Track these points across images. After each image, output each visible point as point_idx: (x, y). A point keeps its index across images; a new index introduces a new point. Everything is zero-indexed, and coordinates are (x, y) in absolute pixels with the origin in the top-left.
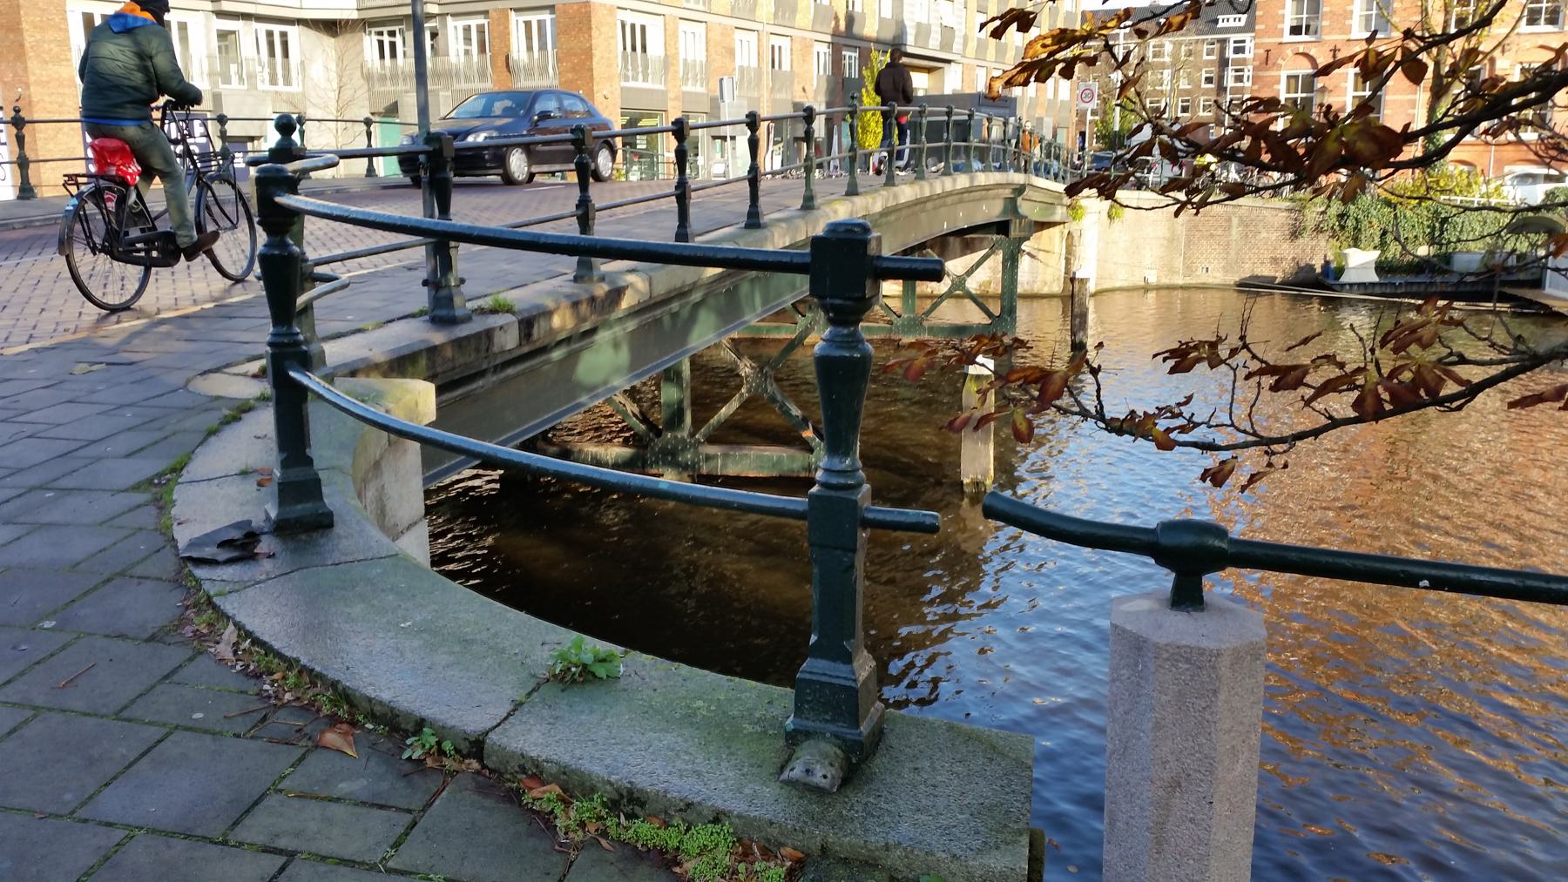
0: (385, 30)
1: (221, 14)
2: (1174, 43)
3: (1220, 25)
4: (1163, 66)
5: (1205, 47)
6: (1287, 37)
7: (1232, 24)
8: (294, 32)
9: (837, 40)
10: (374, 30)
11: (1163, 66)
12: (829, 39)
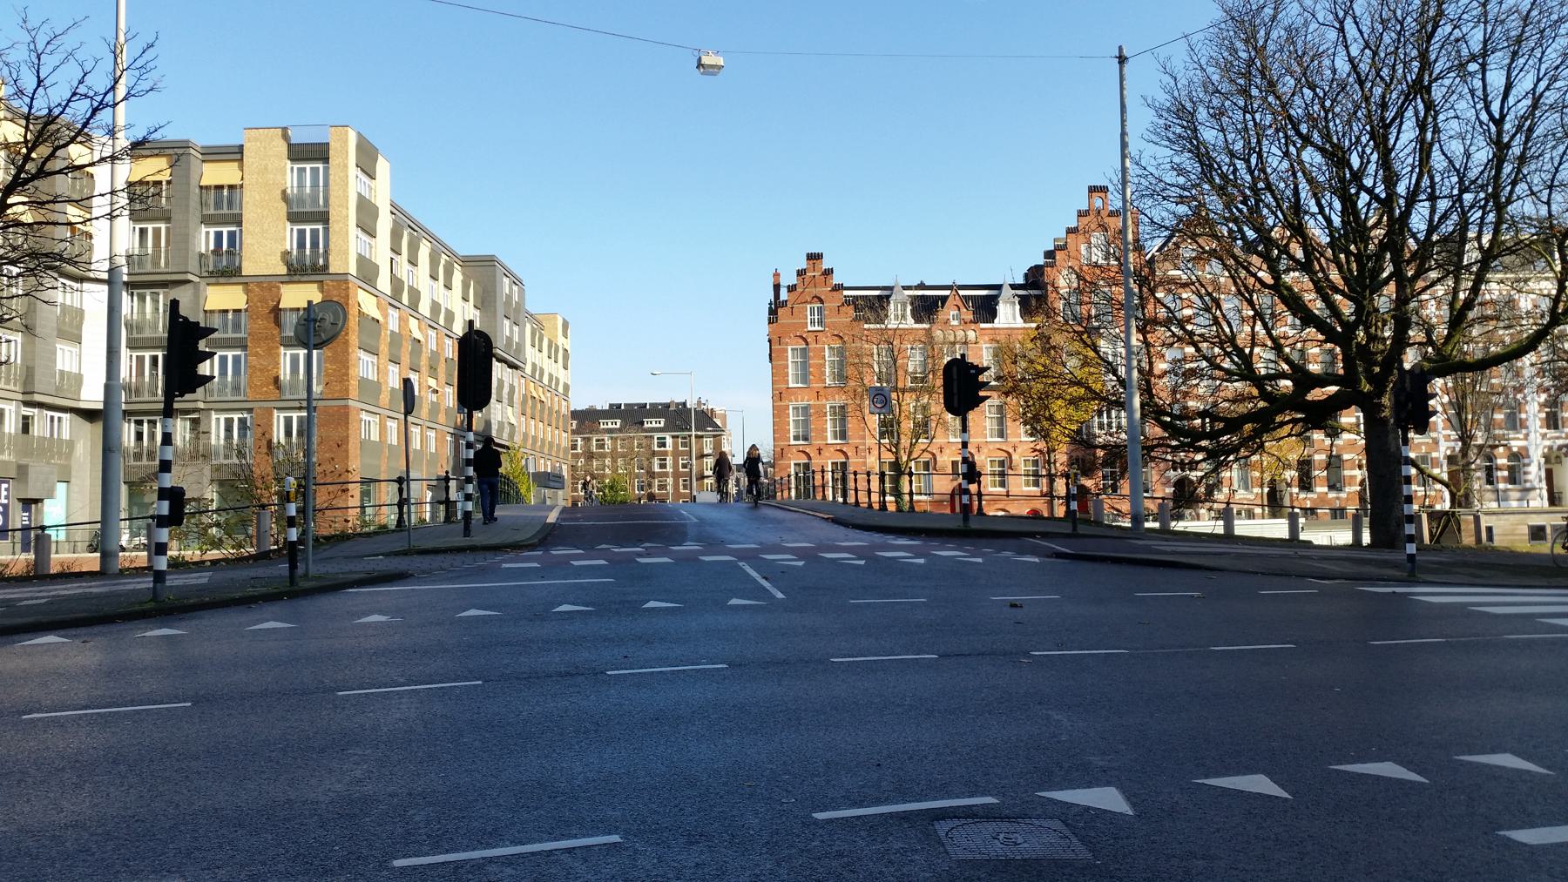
0: (145, 419)
1: (27, 404)
2: (673, 437)
3: (646, 425)
4: (603, 456)
6: (792, 442)
7: (654, 425)
8: (66, 416)
9: (456, 432)
10: (133, 419)
12: (451, 430)
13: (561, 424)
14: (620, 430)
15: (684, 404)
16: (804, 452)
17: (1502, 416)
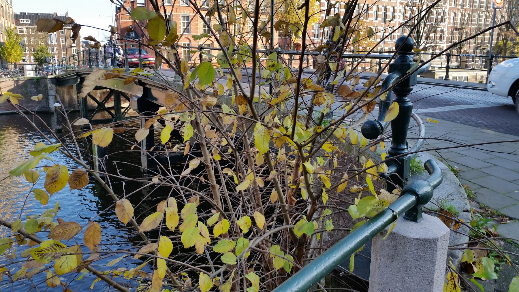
5: (30, 30)
7: (25, 22)
11: (23, 36)
13: (11, 19)
14: (30, 25)
15: (57, 15)
16: (187, 38)
17: (150, 59)
